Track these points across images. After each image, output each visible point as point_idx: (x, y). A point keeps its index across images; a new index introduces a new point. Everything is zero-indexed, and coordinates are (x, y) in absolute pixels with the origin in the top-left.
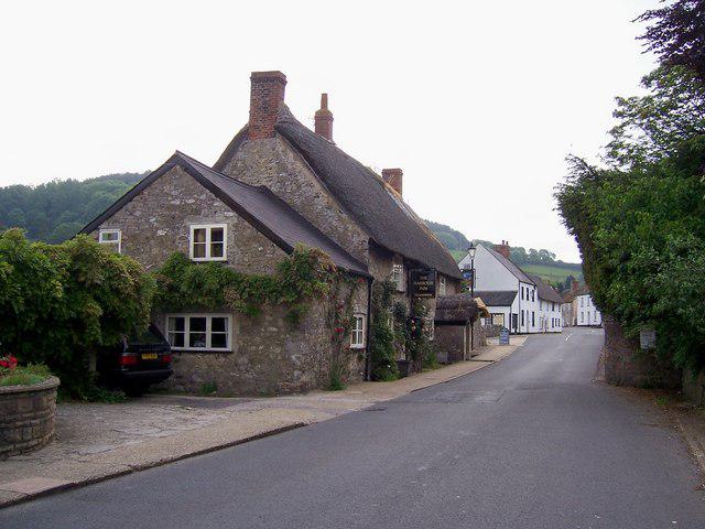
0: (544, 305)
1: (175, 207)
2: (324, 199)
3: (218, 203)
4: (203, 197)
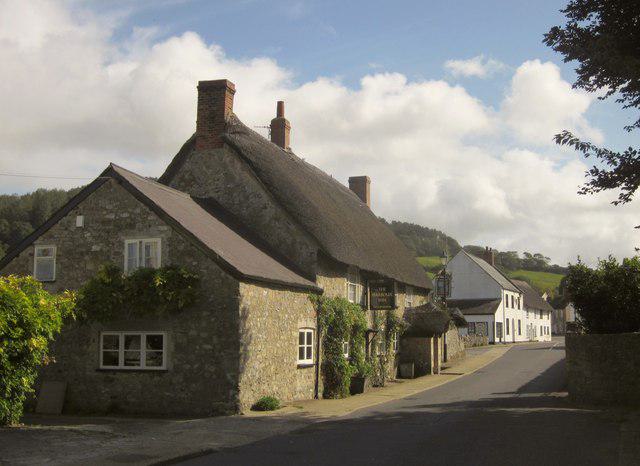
0: (532, 315)
1: (109, 221)
2: (272, 210)
3: (152, 217)
4: (138, 211)
